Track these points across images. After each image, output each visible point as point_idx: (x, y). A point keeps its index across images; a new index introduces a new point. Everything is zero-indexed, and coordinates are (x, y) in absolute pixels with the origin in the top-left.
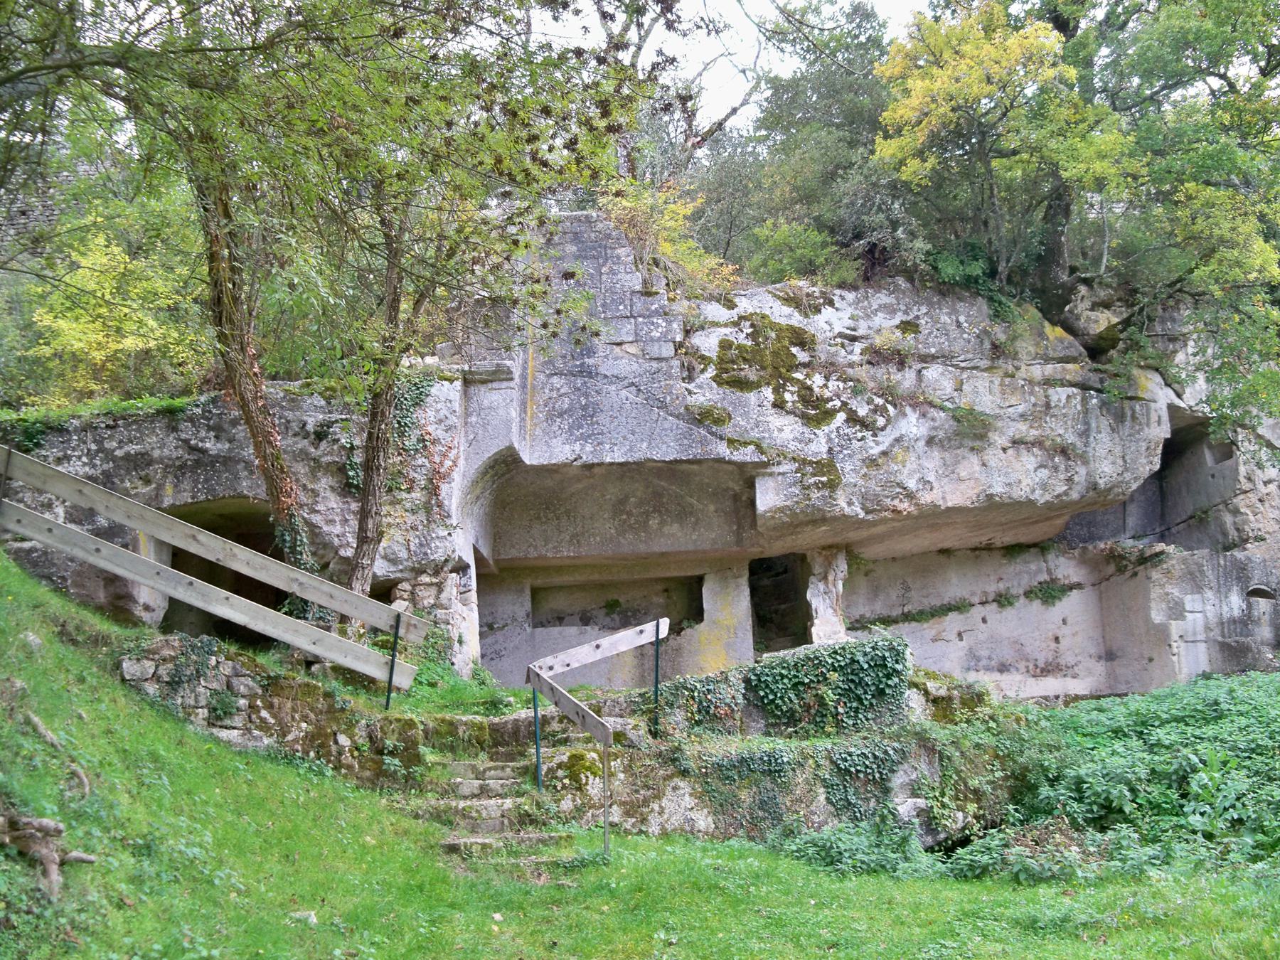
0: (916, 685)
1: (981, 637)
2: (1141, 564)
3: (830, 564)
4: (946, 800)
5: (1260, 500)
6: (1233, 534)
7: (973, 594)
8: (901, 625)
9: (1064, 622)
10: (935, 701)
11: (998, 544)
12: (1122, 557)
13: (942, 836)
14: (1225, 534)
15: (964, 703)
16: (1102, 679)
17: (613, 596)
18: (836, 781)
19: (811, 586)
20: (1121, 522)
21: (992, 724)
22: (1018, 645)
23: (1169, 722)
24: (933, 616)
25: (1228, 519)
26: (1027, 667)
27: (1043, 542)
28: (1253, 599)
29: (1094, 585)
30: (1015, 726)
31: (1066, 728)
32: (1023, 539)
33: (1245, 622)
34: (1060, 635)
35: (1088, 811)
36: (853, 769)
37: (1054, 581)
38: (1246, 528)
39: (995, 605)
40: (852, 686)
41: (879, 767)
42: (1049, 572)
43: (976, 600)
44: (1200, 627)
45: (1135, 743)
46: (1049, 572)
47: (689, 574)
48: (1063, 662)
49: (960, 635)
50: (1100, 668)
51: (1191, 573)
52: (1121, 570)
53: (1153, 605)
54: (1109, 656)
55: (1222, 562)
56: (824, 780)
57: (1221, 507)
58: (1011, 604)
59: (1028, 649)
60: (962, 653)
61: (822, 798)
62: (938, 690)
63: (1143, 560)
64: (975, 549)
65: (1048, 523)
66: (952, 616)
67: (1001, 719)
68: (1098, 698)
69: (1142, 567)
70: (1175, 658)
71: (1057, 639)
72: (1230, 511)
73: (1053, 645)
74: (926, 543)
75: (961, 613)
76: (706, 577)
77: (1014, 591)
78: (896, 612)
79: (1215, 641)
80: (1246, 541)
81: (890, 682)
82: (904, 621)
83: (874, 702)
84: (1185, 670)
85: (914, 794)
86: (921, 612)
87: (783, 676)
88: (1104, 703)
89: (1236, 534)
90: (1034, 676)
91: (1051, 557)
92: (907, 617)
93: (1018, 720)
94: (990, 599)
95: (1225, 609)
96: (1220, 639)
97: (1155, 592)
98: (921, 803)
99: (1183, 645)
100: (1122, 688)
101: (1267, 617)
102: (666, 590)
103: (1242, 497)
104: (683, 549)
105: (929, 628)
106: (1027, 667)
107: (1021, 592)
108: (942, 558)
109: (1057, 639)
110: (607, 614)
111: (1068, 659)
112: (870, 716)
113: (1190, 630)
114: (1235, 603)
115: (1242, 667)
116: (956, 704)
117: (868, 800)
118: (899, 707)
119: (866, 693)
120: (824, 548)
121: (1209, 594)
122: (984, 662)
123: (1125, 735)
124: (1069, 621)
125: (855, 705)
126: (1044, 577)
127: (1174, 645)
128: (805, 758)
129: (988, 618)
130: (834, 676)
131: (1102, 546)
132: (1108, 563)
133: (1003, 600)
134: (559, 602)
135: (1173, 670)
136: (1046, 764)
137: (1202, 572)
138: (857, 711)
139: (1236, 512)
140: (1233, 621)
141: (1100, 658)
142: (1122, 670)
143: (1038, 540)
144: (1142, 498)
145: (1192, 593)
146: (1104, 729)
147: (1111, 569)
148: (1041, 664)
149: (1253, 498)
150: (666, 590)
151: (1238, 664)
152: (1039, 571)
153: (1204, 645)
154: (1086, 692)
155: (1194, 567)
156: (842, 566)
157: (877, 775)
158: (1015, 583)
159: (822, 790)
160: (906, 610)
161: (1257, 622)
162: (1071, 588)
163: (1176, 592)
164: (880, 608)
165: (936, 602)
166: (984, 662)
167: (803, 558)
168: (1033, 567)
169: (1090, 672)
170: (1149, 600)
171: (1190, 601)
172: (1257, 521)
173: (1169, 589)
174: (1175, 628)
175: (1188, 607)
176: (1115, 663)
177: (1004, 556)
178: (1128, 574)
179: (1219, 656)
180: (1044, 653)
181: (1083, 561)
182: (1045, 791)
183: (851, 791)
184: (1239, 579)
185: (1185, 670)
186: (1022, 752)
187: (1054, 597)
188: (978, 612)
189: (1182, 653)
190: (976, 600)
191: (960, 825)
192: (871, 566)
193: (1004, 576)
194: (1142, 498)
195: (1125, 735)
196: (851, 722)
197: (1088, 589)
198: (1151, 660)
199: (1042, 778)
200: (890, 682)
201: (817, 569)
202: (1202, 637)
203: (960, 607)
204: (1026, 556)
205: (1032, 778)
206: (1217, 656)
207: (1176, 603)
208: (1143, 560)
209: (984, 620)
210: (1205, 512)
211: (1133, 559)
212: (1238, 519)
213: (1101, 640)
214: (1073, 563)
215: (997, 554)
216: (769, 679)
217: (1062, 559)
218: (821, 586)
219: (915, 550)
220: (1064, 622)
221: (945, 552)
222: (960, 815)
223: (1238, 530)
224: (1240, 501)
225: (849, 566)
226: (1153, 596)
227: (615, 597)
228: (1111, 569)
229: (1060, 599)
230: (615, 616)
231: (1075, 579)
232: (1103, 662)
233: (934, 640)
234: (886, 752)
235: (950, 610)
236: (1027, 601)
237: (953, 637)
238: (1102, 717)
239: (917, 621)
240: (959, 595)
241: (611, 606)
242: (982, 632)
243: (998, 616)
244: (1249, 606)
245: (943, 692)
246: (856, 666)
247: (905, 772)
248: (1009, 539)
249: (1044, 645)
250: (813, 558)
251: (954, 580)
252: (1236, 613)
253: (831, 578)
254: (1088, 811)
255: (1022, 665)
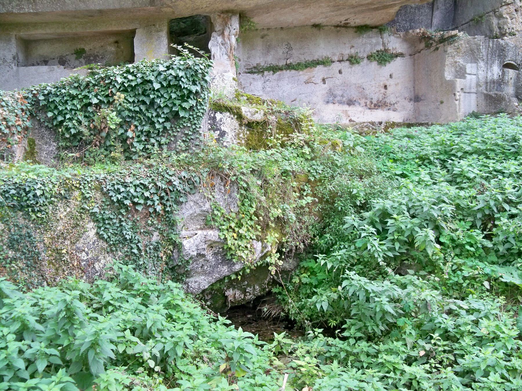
0: (228, 109)
1: (337, 82)
2: (441, 42)
3: (226, 24)
4: (242, 231)
5: (516, 10)
6: (496, 30)
7: (334, 54)
8: (284, 71)
9: (391, 76)
10: (250, 125)
11: (352, 24)
12: (430, 38)
13: (237, 267)
14: (491, 31)
15: (280, 128)
16: (411, 113)
17: (80, 46)
18: (108, 213)
19: (212, 38)
20: (430, 21)
21: (307, 150)
22: (361, 89)
23: (471, 154)
24: (306, 67)
25: (495, 21)
26: (366, 103)
27: (381, 25)
28: (506, 70)
29: (410, 55)
30: (330, 152)
31: (379, 154)
32: (368, 22)
33: (500, 82)
34: (388, 84)
35: (390, 249)
36: (127, 202)
37: (386, 50)
38: (506, 27)
39: (347, 63)
40: (143, 108)
41: (162, 198)
42: (384, 44)
43: (336, 58)
44: (474, 84)
45: (442, 174)
46: (384, 44)
47: (125, 29)
48: (388, 101)
49: (324, 80)
50: (410, 106)
51: (472, 50)
52: (428, 46)
53: (446, 68)
54: (416, 99)
55: (491, 45)
56: (93, 214)
57: (491, 13)
58: (358, 63)
59: (367, 92)
60: (324, 92)
61: (92, 233)
62: (252, 115)
63: (443, 40)
64: (337, 26)
65: (384, 11)
66: (320, 68)
67: (316, 145)
68: (409, 126)
69: (442, 44)
70: (457, 102)
71: (385, 87)
72: (496, 16)
73: (383, 90)
74: (302, 17)
75: (325, 66)
76: (137, 31)
77: (360, 55)
78: (282, 63)
79: (482, 93)
80: (504, 35)
81: (185, 105)
82: (286, 69)
83: (168, 125)
84: (462, 110)
85: (207, 225)
86: (299, 64)
87: (73, 97)
88: (413, 131)
89: (498, 30)
90: (370, 109)
91: (386, 35)
92: (289, 67)
93: (334, 146)
94: (345, 59)
95: (489, 74)
96: (485, 92)
97: (449, 61)
98: (213, 235)
99: (463, 94)
100: (422, 120)
101: (512, 81)
102: (116, 42)
103: (505, 7)
104: (112, 7)
105: (304, 75)
106: (366, 103)
107: (365, 56)
108: (315, 30)
109: (385, 87)
110: (77, 59)
111: (392, 99)
112: (163, 140)
113: (468, 85)
114: (496, 70)
115: (498, 110)
116: (272, 128)
117: (149, 233)
118: (195, 131)
119: (158, 116)
120: (222, 12)
121: (482, 64)
122: (338, 98)
123: (431, 163)
124: (394, 76)
125: (146, 128)
126: (380, 48)
127: (458, 94)
128: (69, 190)
129: (343, 71)
130: (120, 97)
131: (418, 31)
132: (420, 42)
133: (353, 60)
134: (44, 50)
135: (455, 110)
136: (355, 191)
137: (479, 49)
138: (148, 134)
139: (500, 17)
140: (493, 82)
141: (411, 100)
142: (423, 107)
143: (378, 24)
144: (444, 8)
145: (471, 62)
146: (412, 156)
147: (422, 45)
148: (375, 101)
149: (512, 8)
150: (116, 42)
151: (495, 108)
152: (377, 44)
153: (475, 95)
154: (400, 121)
155: (474, 47)
156: (235, 24)
157: (159, 208)
158: (362, 50)
159: (91, 224)
160: (288, 62)
161: (507, 84)
162: (397, 56)
163: (461, 61)
164: (270, 60)
165: (310, 58)
166: (338, 98)
167: (207, 19)
168: (374, 41)
169: (404, 108)
170: (444, 65)
171: (470, 68)
172: (512, 23)
173: (457, 59)
174: (459, 83)
175: (468, 71)
176: (420, 103)
177: (356, 32)
178: (432, 49)
179: (484, 103)
180: (377, 95)
181: (406, 39)
182: (351, 219)
183: (127, 225)
184: (499, 56)
185: (462, 110)
186: (333, 177)
187: (386, 61)
188: (336, 66)
189: (462, 99)
190: (336, 58)
191: (258, 255)
192: (265, 32)
193: (355, 45)
194: (444, 8)
195: (431, 163)
196: (141, 147)
197: (407, 57)
198: (442, 102)
199: (349, 205)
200: (185, 105)
201: (218, 28)
202: (474, 90)
203: (325, 62)
204: (370, 33)
205: (339, 205)
206: (483, 103)
207: (461, 68)
208: (443, 40)
209: (340, 72)
210: (481, 17)
211: (436, 39)
212: (501, 21)
213: (412, 89)
214: (400, 40)
215: (351, 31)
216: (57, 99)
217: (392, 38)
218: (220, 39)
219: (295, 23)
220: (391, 76)
221: (316, 26)
222: (258, 246)
223: (500, 28)
224: (504, 10)
225: (241, 26)
226: (447, 63)
227: (82, 46)
228: (422, 45)
229: (389, 62)
230: (82, 60)
231: (399, 51)
232: (412, 102)
233: (307, 82)
234: (170, 182)
235: (318, 64)
236: (368, 62)
237: (319, 81)
238: (411, 144)
239: (295, 69)
240: (325, 55)
241: (79, 53)
242: (339, 79)
243: (350, 70)
244: (504, 73)
245: (259, 117)
246: (148, 87)
247: (196, 203)
248: (358, 20)
249: (377, 90)
250: (215, 20)
251: (322, 45)
252: (496, 77)
253: (226, 33)
254: (390, 249)
255: (362, 102)
